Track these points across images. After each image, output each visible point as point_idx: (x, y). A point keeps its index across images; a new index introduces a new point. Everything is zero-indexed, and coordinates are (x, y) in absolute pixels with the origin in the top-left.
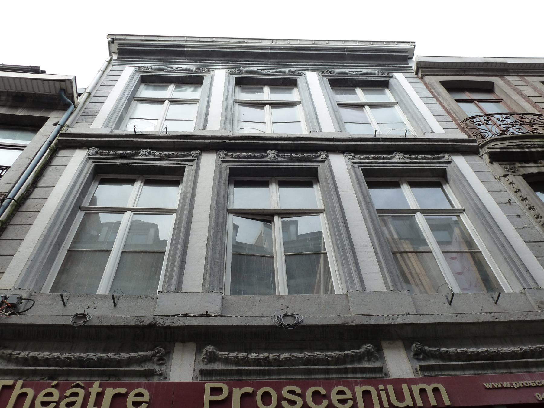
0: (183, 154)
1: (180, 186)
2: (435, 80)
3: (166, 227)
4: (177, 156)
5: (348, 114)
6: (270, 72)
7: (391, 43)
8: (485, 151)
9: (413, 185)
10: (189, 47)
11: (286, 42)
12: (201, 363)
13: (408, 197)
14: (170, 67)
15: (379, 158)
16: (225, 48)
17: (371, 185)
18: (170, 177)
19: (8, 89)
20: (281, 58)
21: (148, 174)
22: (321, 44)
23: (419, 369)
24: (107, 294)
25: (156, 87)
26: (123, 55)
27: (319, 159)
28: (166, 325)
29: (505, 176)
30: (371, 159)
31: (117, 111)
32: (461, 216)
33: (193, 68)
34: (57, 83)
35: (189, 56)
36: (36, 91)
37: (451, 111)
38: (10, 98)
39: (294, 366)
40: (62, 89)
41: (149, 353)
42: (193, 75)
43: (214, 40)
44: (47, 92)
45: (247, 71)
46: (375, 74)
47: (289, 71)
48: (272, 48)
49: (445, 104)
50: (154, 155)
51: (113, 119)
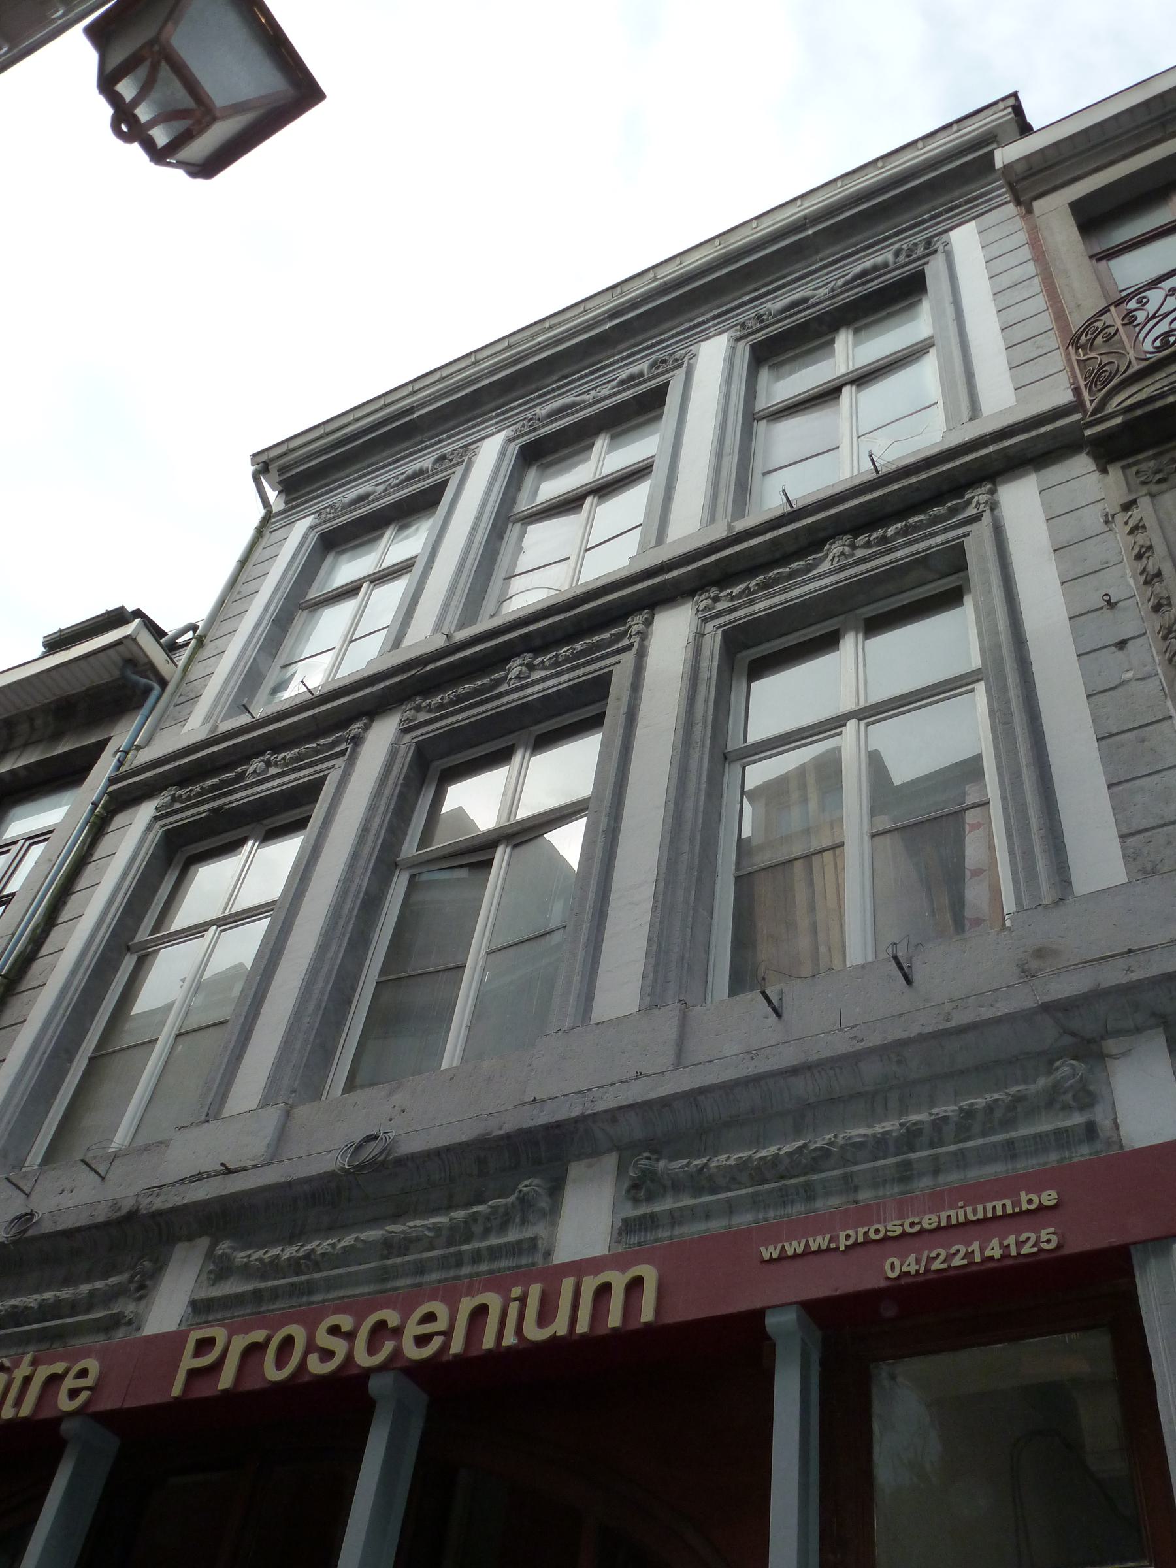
0: (328, 740)
1: (968, 601)
3: (962, 731)
4: (317, 752)
6: (606, 391)
7: (939, 135)
10: (424, 405)
14: (818, 287)
15: (776, 581)
18: (936, 587)
20: (644, 330)
21: (271, 816)
22: (668, 274)
24: (870, 959)
26: (297, 491)
27: (971, 511)
28: (154, 1208)
30: (755, 592)
31: (242, 664)
34: (111, 652)
41: (124, 1277)
47: (897, 254)
48: (614, 314)
51: (228, 691)
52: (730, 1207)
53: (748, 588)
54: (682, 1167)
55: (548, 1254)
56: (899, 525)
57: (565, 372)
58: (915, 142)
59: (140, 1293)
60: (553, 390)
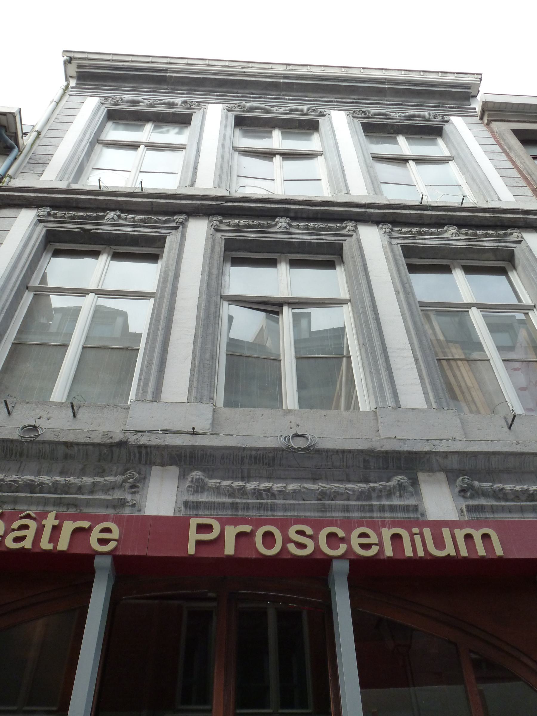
0: (163, 218)
1: (160, 263)
3: (139, 317)
4: (156, 222)
5: (386, 171)
6: (282, 110)
10: (174, 72)
13: (461, 286)
18: (145, 249)
20: (298, 91)
33: (179, 101)
41: (119, 478)
42: (177, 111)
43: (207, 62)
45: (251, 108)
47: (308, 109)
48: (285, 77)
50: (125, 219)
52: (522, 509)
54: (490, 486)
55: (140, 510)
58: (438, 72)
59: (134, 490)
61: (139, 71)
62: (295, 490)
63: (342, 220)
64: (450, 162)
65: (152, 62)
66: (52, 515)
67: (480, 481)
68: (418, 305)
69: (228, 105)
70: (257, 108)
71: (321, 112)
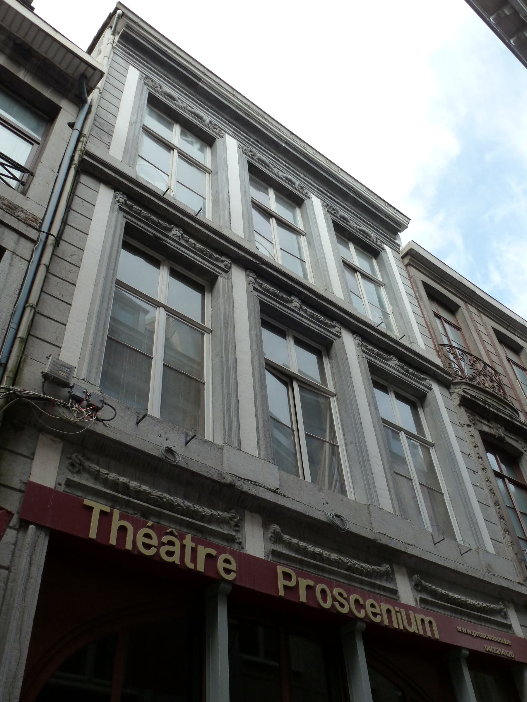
2: (420, 277)
5: (148, 146)
6: (280, 174)
7: (402, 216)
8: (457, 390)
9: (174, 273)
10: (205, 84)
11: (303, 144)
12: (269, 541)
13: (159, 283)
16: (241, 110)
17: (126, 246)
19: (14, 30)
23: (418, 600)
25: (160, 119)
26: (126, 42)
29: (469, 426)
32: (331, 399)
33: (207, 118)
35: (199, 94)
36: (49, 56)
37: (430, 326)
38: (11, 44)
39: (339, 568)
40: (83, 76)
41: (225, 515)
42: (200, 125)
43: (235, 93)
44: (63, 67)
45: (259, 159)
46: (294, 184)
48: (287, 143)
49: (425, 313)
50: (187, 241)
53: (195, 245)
56: (414, 372)
57: (260, 141)
59: (237, 529)
60: (258, 146)
61: (178, 66)
62: (336, 559)
63: (222, 254)
64: (207, 174)
65: (191, 64)
66: (189, 537)
67: (425, 581)
68: (114, 281)
69: (242, 145)
70: (263, 162)
71: (307, 193)
